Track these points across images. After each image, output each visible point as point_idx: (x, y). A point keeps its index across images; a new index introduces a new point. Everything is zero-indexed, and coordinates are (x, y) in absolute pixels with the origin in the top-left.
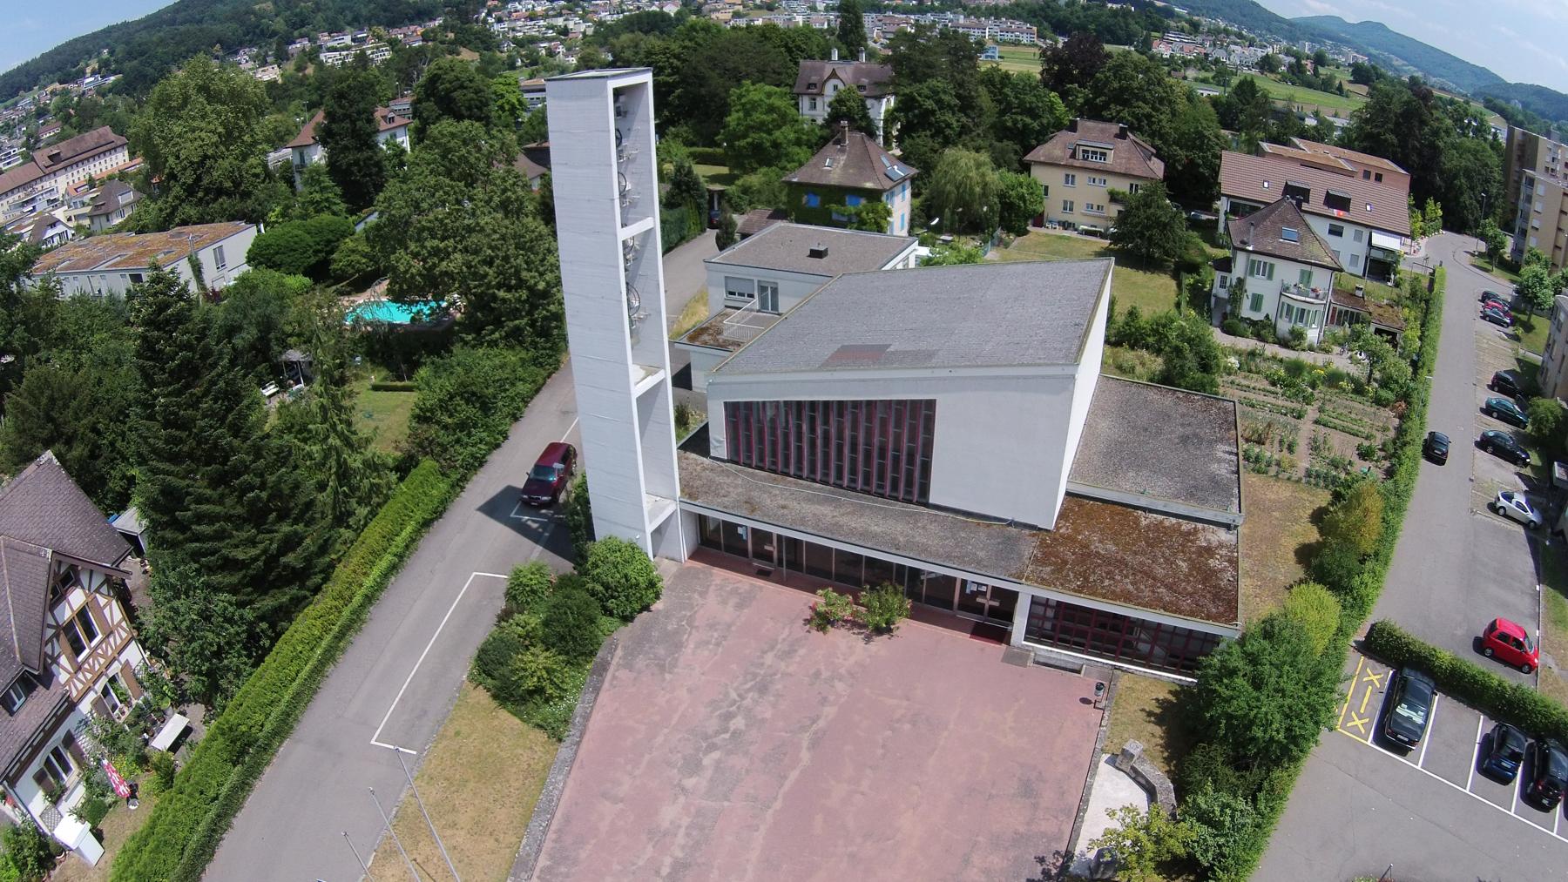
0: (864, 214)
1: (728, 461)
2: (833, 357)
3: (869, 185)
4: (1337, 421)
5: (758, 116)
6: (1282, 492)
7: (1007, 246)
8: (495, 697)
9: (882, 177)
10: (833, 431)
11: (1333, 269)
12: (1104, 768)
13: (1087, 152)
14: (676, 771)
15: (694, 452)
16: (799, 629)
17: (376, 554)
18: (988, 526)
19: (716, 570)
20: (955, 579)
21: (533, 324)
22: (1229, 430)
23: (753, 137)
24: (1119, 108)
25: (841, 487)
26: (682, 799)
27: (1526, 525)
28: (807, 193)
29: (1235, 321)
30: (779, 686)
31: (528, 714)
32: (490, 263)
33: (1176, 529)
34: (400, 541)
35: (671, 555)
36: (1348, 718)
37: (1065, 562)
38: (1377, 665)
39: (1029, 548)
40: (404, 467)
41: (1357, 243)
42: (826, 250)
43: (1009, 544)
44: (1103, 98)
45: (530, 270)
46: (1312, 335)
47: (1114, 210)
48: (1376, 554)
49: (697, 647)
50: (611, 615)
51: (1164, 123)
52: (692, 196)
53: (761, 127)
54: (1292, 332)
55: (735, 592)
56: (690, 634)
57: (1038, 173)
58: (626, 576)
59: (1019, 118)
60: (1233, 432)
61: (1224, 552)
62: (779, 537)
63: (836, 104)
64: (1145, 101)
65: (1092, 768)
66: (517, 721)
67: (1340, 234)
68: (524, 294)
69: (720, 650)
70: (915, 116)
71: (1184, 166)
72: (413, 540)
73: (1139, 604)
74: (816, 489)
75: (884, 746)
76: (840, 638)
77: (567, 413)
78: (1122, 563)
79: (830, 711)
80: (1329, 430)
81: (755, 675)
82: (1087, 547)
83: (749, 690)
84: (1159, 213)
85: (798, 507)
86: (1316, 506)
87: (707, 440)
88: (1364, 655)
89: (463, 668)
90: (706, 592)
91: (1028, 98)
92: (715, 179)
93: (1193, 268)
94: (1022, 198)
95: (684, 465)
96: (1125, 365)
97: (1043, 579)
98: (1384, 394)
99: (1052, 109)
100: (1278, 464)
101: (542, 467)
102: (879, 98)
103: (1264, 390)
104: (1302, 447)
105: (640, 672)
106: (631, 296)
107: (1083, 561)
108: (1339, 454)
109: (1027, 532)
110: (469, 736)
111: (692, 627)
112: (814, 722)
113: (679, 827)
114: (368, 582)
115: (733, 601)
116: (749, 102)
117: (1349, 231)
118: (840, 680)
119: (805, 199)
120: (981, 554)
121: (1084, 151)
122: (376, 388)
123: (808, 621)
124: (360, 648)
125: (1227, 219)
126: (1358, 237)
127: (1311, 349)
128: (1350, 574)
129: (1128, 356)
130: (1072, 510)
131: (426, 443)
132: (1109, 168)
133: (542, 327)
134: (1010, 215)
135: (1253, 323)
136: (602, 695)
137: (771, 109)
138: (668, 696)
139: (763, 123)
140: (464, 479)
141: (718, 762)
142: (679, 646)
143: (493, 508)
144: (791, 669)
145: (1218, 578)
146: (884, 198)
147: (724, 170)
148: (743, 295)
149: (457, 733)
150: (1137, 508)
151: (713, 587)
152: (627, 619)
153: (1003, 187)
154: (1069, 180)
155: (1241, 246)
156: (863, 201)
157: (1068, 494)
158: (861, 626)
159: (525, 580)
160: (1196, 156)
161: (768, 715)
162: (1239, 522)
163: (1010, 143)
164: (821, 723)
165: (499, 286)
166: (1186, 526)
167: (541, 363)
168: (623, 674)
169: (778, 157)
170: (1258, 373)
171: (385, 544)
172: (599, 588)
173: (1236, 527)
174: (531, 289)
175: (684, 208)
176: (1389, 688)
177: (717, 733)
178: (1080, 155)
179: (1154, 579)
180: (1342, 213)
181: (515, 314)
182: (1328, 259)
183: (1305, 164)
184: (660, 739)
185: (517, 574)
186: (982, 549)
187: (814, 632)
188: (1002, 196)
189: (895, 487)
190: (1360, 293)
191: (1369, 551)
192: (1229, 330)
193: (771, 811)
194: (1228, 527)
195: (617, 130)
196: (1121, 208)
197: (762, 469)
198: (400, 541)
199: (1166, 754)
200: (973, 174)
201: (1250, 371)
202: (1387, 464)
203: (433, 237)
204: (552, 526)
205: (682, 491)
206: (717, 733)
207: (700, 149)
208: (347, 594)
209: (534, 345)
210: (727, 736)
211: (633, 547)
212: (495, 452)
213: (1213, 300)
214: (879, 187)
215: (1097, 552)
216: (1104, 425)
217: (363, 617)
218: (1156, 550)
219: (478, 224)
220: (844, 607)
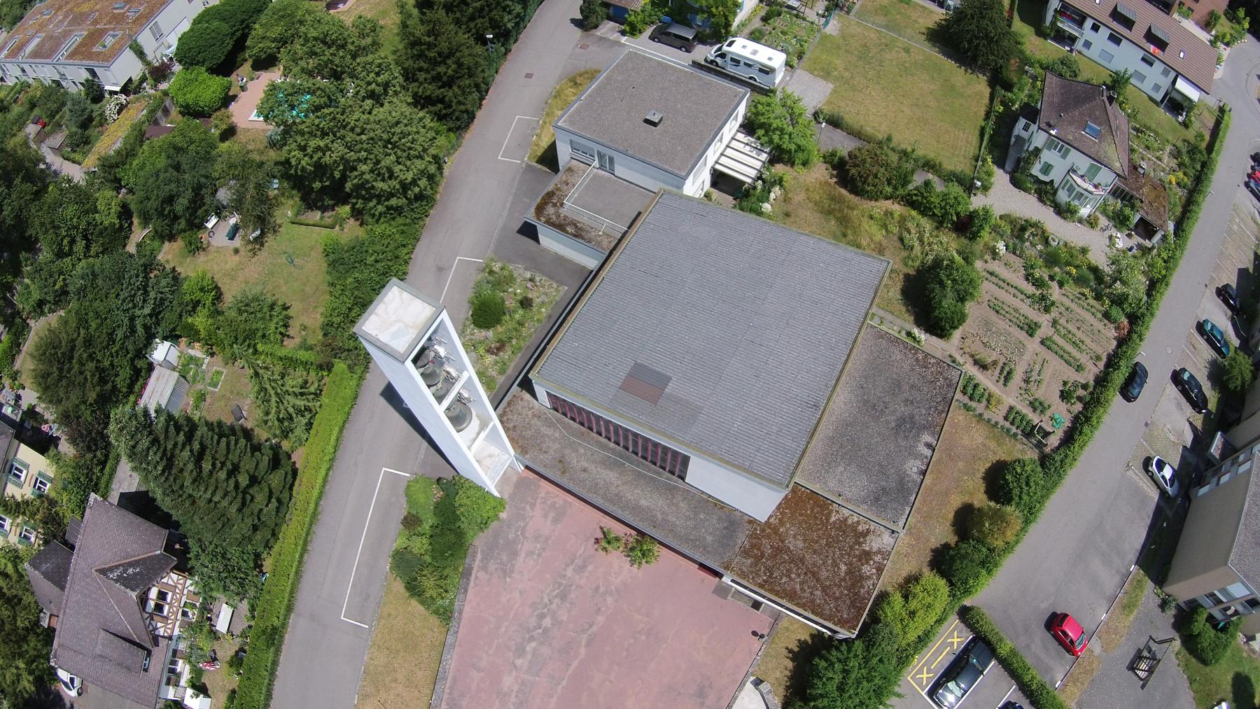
12: (749, 686)
14: (511, 653)
26: (514, 673)
27: (1163, 493)
30: (573, 596)
36: (920, 671)
39: (742, 539)
46: (1084, 211)
49: (527, 556)
55: (553, 506)
61: (878, 558)
65: (742, 684)
66: (422, 608)
69: (541, 560)
75: (627, 650)
79: (601, 619)
80: (1049, 355)
81: (560, 584)
82: (783, 542)
105: (491, 575)
110: (396, 617)
111: (524, 537)
112: (591, 627)
113: (512, 691)
115: (552, 515)
120: (709, 539)
127: (1080, 221)
135: (1037, 181)
136: (469, 593)
141: (535, 649)
142: (514, 554)
149: (389, 615)
151: (539, 501)
161: (565, 618)
164: (594, 628)
168: (481, 575)
170: (1020, 257)
177: (535, 628)
179: (817, 580)
180: (1157, 51)
182: (1118, 164)
184: (503, 630)
186: (711, 534)
192: (1016, 183)
193: (560, 687)
199: (788, 684)
206: (535, 628)
210: (541, 631)
213: (1013, 140)
215: (789, 548)
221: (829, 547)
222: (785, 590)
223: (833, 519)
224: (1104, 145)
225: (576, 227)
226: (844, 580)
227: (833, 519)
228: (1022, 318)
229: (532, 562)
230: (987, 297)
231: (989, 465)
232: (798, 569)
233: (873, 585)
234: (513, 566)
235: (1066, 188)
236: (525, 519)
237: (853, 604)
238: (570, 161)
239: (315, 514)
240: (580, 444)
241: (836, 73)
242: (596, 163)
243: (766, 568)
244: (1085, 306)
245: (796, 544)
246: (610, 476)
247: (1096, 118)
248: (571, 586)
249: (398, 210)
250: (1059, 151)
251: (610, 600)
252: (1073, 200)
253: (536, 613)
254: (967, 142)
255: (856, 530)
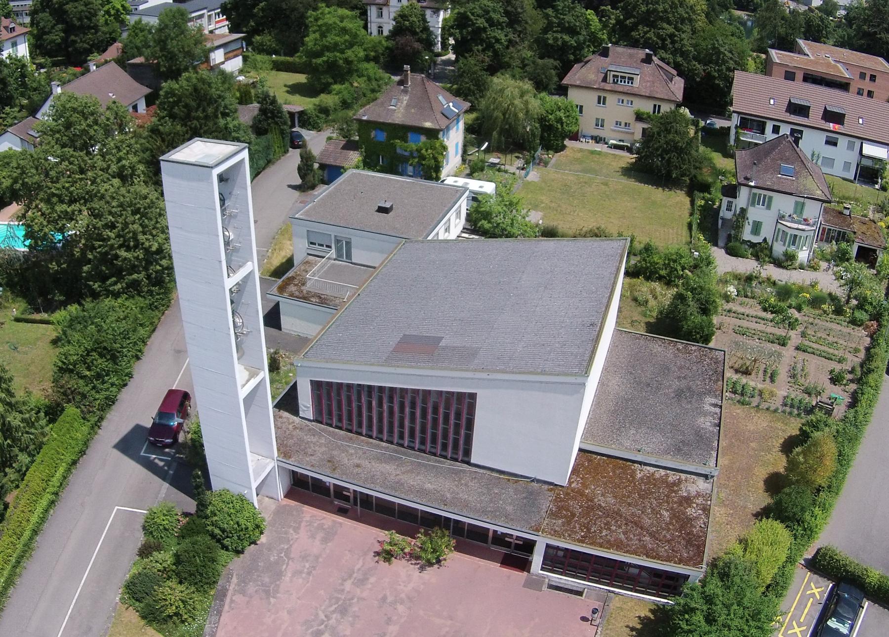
0: (423, 151)
1: (313, 421)
2: (396, 350)
3: (428, 125)
4: (815, 346)
5: (331, 38)
6: (759, 423)
7: (546, 164)
8: (143, 617)
9: (439, 116)
10: (396, 408)
11: (823, 201)
13: (617, 76)
15: (287, 410)
16: (370, 559)
17: (38, 495)
18: (516, 482)
19: (306, 508)
20: (489, 529)
21: (149, 277)
22: (718, 380)
23: (328, 56)
24: (646, 29)
25: (402, 446)
28: (375, 129)
29: (738, 244)
30: (355, 609)
31: (169, 631)
32: (112, 226)
33: (664, 480)
34: (55, 481)
35: (271, 495)
37: (573, 515)
38: (820, 579)
39: (546, 503)
40: (53, 413)
41: (849, 152)
42: (392, 206)
43: (531, 497)
44: (632, 20)
45: (144, 233)
46: (803, 255)
47: (638, 129)
48: (829, 487)
49: (293, 575)
50: (227, 550)
51: (685, 42)
52: (277, 123)
53: (335, 47)
54: (786, 254)
55: (321, 527)
56: (288, 564)
57: (575, 97)
58: (237, 523)
59: (559, 36)
60: (720, 383)
61: (700, 501)
62: (355, 491)
63: (400, 19)
64: (669, 23)
67: (835, 144)
68: (140, 254)
69: (311, 578)
70: (468, 33)
71: (701, 78)
72: (65, 478)
73: (627, 552)
74: (382, 448)
76: (402, 568)
77: (180, 353)
78: (618, 513)
80: (807, 356)
81: (338, 599)
82: (592, 501)
83: (334, 612)
84: (677, 138)
85: (369, 466)
86: (786, 435)
87: (295, 398)
88: (810, 571)
89: (116, 595)
90: (299, 528)
91: (567, 18)
92: (295, 89)
93: (705, 188)
94: (560, 120)
95: (279, 425)
96: (640, 298)
97: (555, 531)
98: (859, 315)
99: (588, 24)
100: (761, 393)
101: (163, 413)
102: (436, 11)
103: (756, 317)
104: (783, 375)
105: (251, 597)
106: (235, 317)
107: (588, 514)
108: (813, 382)
109: (546, 487)
111: (289, 559)
114: (34, 519)
115: (320, 535)
116: (325, 24)
117: (843, 142)
118: (401, 604)
119: (373, 134)
120: (509, 508)
121: (614, 76)
122: (18, 320)
123: (377, 554)
124: (33, 568)
125: (737, 133)
126: (851, 147)
127: (801, 267)
128: (803, 510)
129: (644, 288)
130: (583, 465)
131: (69, 391)
132: (635, 91)
133: (156, 278)
134: (549, 135)
135: (753, 245)
137: (344, 31)
138: (273, 617)
139: (336, 44)
140: (101, 419)
142: (279, 575)
143: (126, 446)
144: (365, 594)
145: (692, 526)
146: (440, 135)
147: (301, 78)
148: (322, 245)
150: (634, 462)
151: (303, 524)
152: (239, 552)
153: (544, 113)
154: (601, 101)
155: (745, 182)
156: (423, 138)
157: (580, 450)
158: (418, 558)
159: (159, 521)
160: (712, 69)
162: (716, 474)
163: (552, 61)
165: (120, 247)
166: (673, 477)
167: (156, 307)
168: (238, 598)
169: (350, 72)
170: (753, 298)
171: (44, 485)
172: (217, 531)
173: (712, 477)
174: (147, 251)
175: (269, 136)
176: (827, 600)
178: (610, 79)
179: (642, 528)
180: (837, 126)
181: (133, 269)
182: (819, 192)
183: (811, 78)
185: (152, 515)
186: (510, 504)
187: (381, 563)
188: (542, 120)
189: (445, 447)
190: (847, 212)
191: (823, 485)
192: (732, 252)
194: (706, 477)
195: (220, 194)
196: (646, 126)
197: (340, 428)
198: (55, 481)
200: (517, 102)
201: (746, 296)
202: (853, 387)
203: (62, 201)
204: (175, 465)
205: (278, 450)
207: (282, 58)
208: (18, 531)
209: (150, 292)
211: (242, 499)
212: (124, 390)
213: (720, 222)
214: (438, 127)
215: (600, 505)
216: (614, 382)
217: (31, 546)
218: (646, 501)
219: (99, 191)
220: (408, 543)
221: (644, 499)
222: (608, 542)
223: (639, 476)
224: (801, 180)
225: (320, 298)
226: (671, 523)
227: (639, 476)
228: (771, 336)
229: (301, 581)
230: (731, 327)
231: (783, 440)
232: (617, 522)
233: (704, 523)
234: (278, 586)
235: (779, 238)
236: (289, 541)
237: (689, 542)
238: (306, 257)
239: (28, 548)
240: (349, 446)
241: (543, 205)
242: (333, 253)
243: (581, 524)
244: (829, 319)
245: (605, 500)
246: (389, 468)
247: (788, 159)
248: (352, 599)
249: (135, 285)
250: (763, 205)
251: (401, 608)
252: (789, 246)
253: (310, 631)
254: (677, 234)
255: (667, 483)
